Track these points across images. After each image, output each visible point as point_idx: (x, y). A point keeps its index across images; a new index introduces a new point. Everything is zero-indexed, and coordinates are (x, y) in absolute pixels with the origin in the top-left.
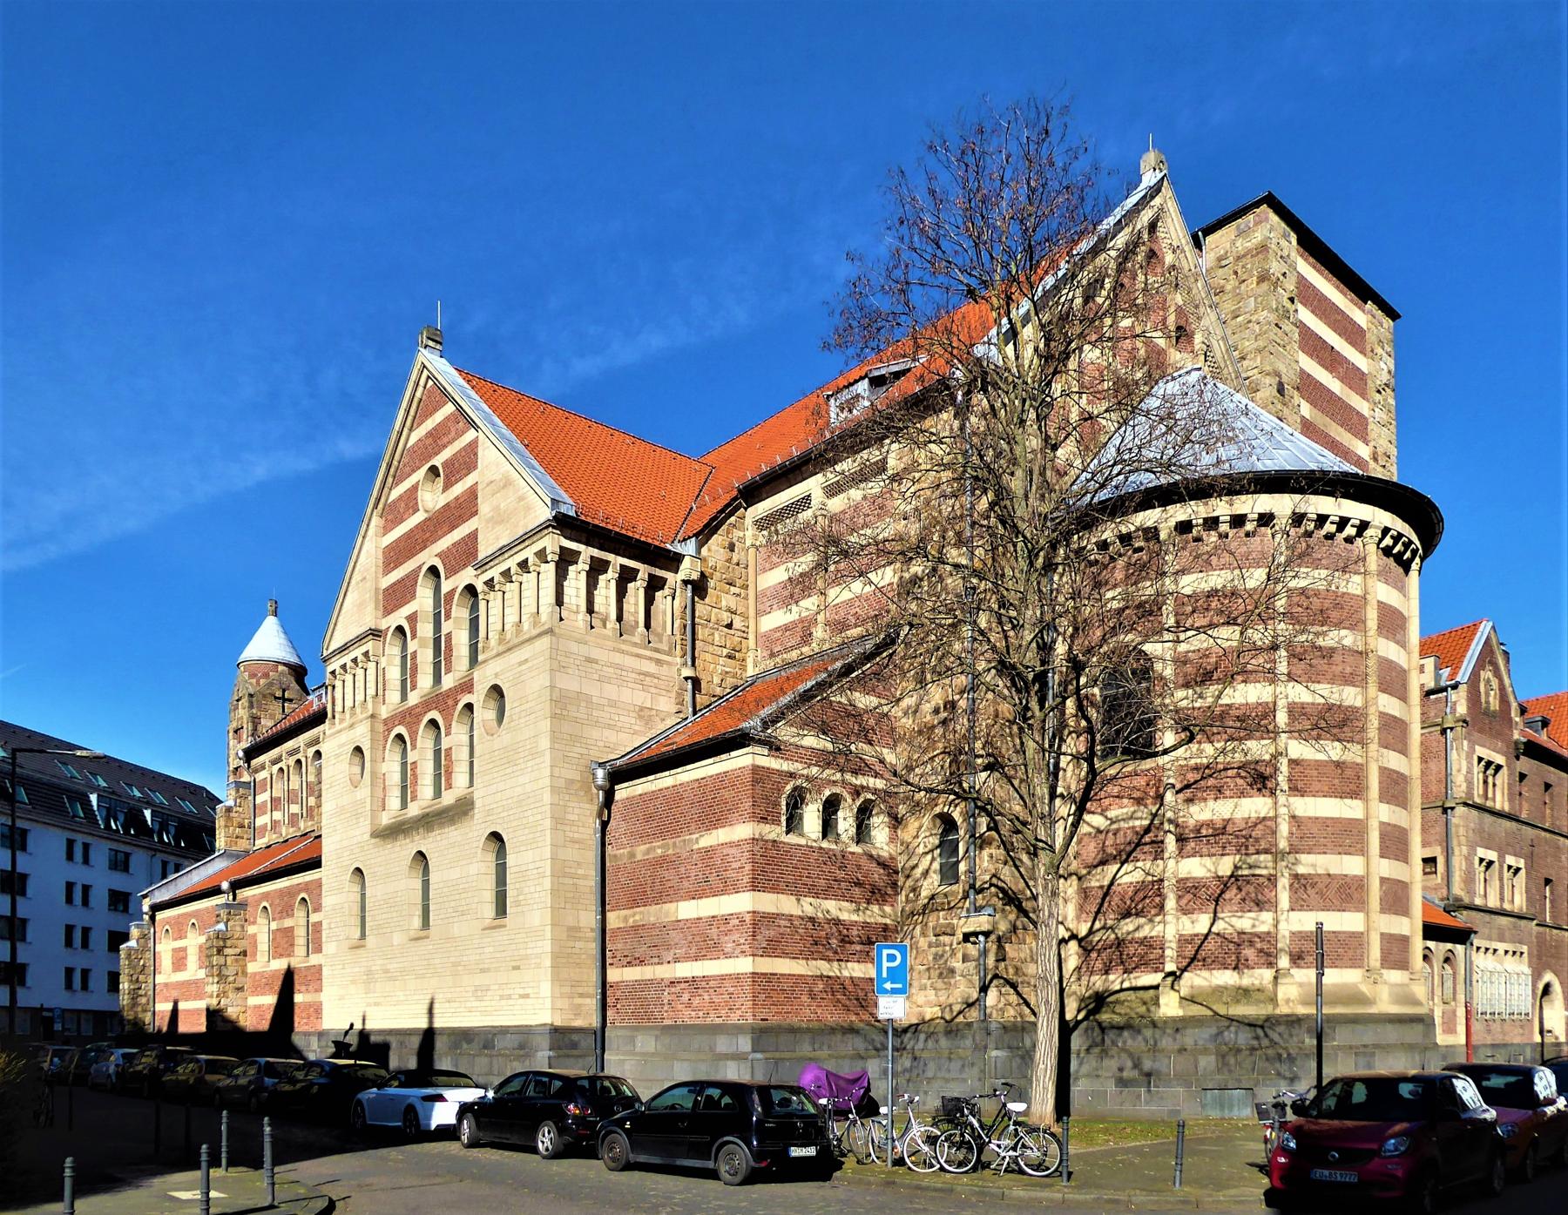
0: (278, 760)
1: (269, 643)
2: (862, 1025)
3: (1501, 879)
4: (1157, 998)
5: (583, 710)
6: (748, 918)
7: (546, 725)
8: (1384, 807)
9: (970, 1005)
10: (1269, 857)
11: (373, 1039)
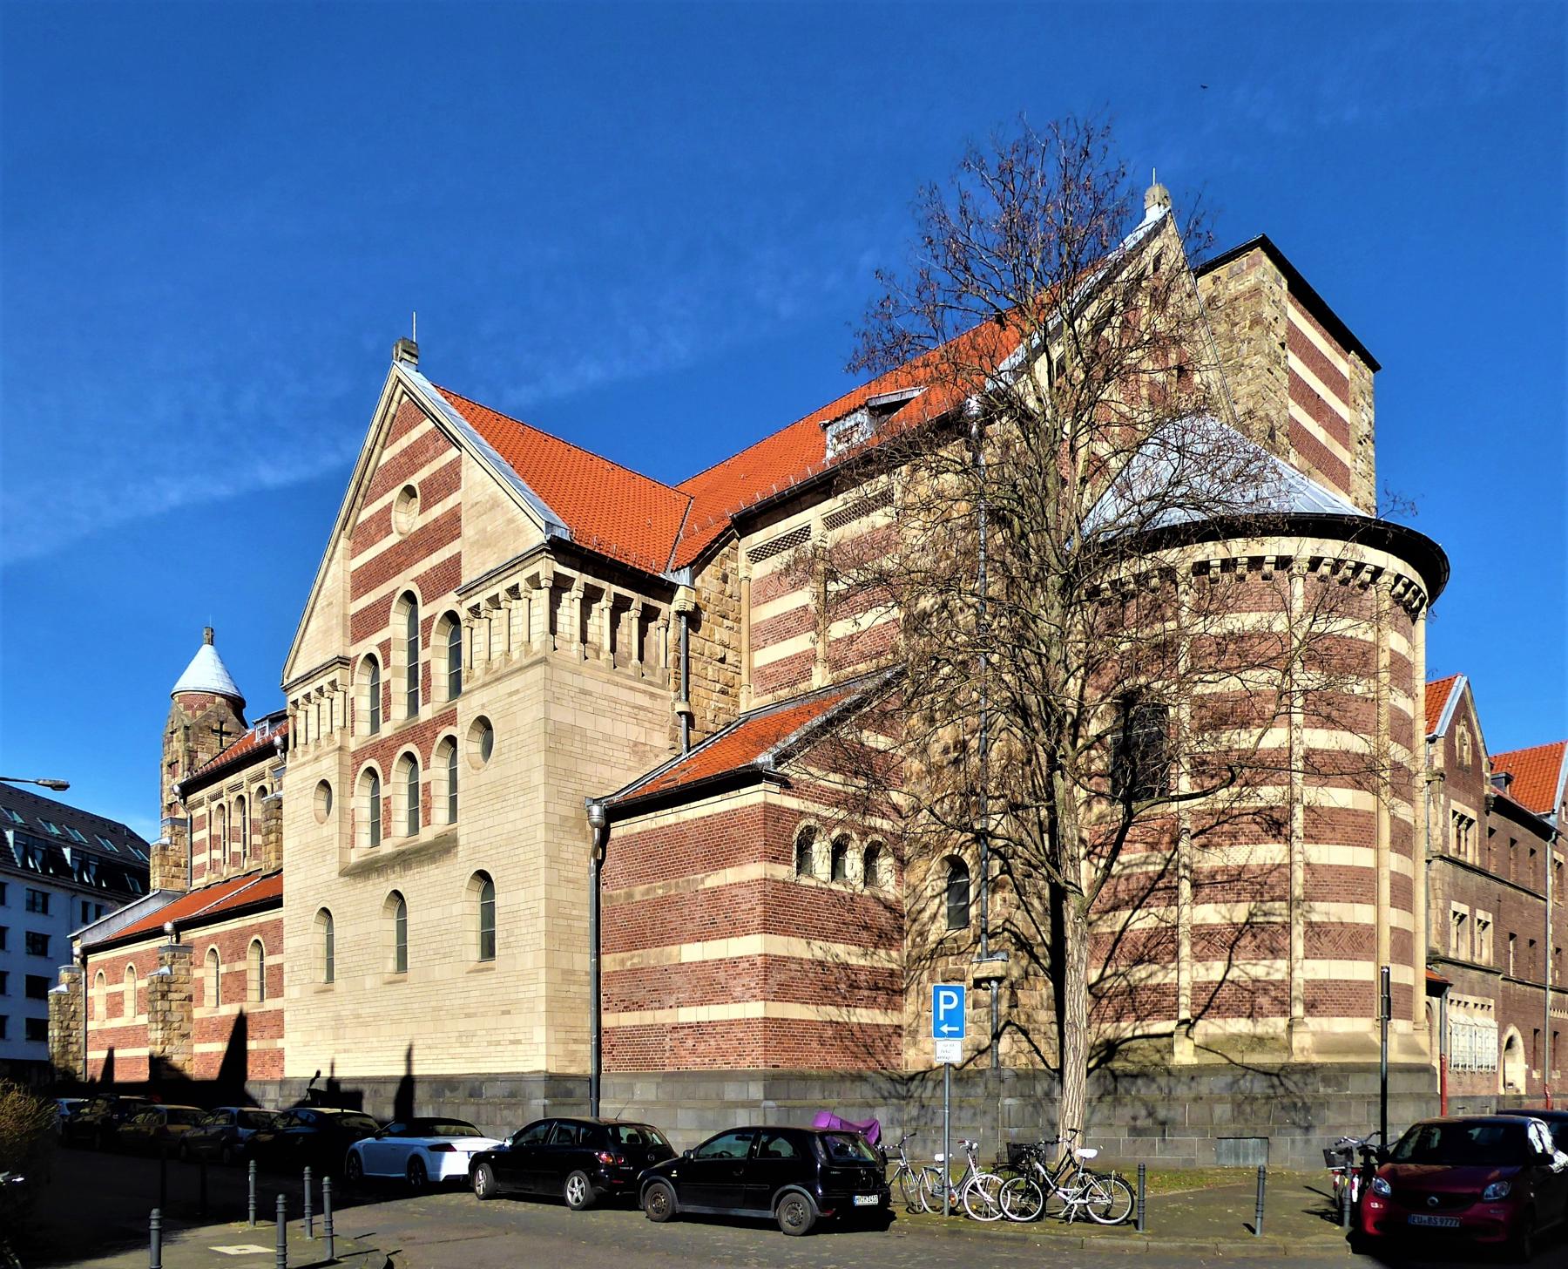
0: (219, 795)
1: (204, 672)
2: (869, 1073)
3: (1472, 933)
4: (1172, 1047)
5: (577, 744)
6: (759, 961)
7: (539, 759)
8: (1394, 856)
9: (981, 1052)
10: (1284, 904)
11: (343, 1087)
